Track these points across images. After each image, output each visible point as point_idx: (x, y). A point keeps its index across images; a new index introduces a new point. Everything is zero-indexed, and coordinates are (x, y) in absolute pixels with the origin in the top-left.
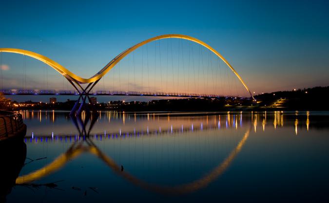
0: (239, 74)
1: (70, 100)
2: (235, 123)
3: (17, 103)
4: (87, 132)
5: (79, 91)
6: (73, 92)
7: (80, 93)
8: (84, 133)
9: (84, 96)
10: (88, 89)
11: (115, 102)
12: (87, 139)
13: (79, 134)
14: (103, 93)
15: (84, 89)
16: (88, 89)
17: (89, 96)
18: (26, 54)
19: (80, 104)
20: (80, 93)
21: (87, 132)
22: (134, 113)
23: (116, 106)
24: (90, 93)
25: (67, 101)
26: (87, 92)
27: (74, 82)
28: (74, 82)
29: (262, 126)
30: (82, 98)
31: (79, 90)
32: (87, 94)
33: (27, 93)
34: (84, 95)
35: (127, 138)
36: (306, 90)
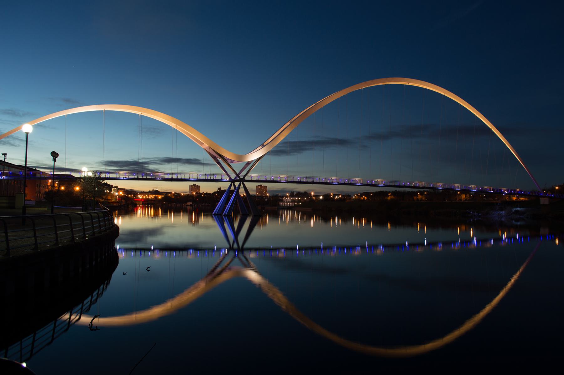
0: (506, 234)
6: (218, 177)
7: (230, 178)
8: (235, 246)
9: (237, 184)
10: (244, 173)
11: (299, 194)
13: (228, 246)
14: (401, 184)
16: (244, 173)
17: (245, 183)
20: (230, 178)
21: (241, 244)
22: (458, 201)
23: (299, 201)
24: (246, 178)
25: (216, 190)
26: (242, 177)
27: (220, 160)
28: (220, 160)
30: (234, 185)
32: (243, 180)
34: (237, 181)
36: (372, 193)
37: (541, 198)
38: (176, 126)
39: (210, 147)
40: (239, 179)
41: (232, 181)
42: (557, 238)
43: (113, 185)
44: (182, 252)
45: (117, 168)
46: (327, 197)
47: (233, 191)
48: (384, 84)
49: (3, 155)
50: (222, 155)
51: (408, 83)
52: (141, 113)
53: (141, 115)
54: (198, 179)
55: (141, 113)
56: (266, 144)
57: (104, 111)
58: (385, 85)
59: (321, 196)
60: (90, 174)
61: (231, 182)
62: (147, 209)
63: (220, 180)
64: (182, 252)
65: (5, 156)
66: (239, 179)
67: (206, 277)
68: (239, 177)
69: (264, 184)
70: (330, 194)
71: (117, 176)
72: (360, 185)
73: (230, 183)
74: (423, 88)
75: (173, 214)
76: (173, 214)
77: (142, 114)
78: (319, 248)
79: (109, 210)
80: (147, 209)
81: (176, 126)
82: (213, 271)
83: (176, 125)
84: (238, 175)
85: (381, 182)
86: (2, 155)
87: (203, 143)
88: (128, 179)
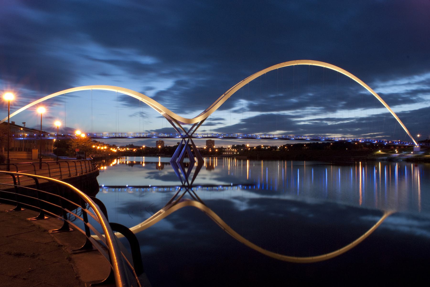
9: (187, 139)
27: (174, 122)
28: (174, 122)
32: (191, 137)
37: (189, 144)
38: (142, 99)
39: (166, 114)
40: (188, 136)
41: (184, 138)
42: (248, 179)
43: (100, 142)
44: (122, 189)
45: (410, 135)
46: (259, 148)
47: (183, 145)
48: (294, 65)
49: (23, 123)
50: (176, 120)
51: (311, 64)
52: (117, 91)
53: (117, 92)
54: (134, 137)
55: (117, 91)
56: (207, 110)
57: (91, 90)
58: (295, 65)
59: (118, 147)
60: (83, 136)
61: (182, 138)
62: (229, 159)
63: (127, 137)
64: (122, 189)
65: (24, 124)
66: (188, 136)
67: (166, 206)
68: (188, 135)
69: (212, 139)
70: (261, 146)
71: (164, 136)
72: (293, 140)
73: (181, 139)
74: (323, 67)
75: (242, 160)
76: (242, 160)
77: (118, 92)
78: (125, 187)
79: (92, 159)
80: (229, 159)
81: (142, 99)
82: (170, 202)
83: (142, 98)
84: (187, 134)
85: (293, 136)
86: (22, 123)
87: (162, 111)
88: (109, 138)
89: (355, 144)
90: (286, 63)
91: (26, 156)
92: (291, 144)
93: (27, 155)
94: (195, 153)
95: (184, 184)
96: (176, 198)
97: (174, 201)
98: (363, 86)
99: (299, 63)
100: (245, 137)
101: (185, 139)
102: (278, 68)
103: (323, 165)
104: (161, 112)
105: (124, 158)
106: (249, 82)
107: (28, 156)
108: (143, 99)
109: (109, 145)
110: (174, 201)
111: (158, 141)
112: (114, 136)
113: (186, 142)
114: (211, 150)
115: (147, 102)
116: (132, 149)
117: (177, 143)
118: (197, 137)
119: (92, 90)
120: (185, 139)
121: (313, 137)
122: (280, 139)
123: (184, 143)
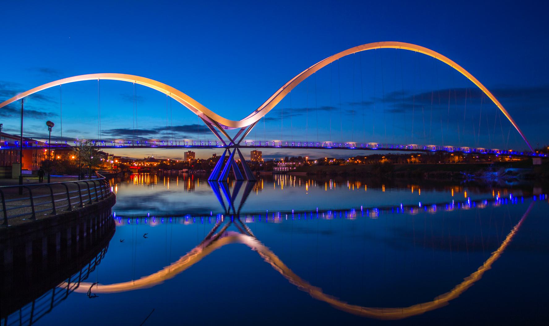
1: (103, 151)
2: (357, 184)
3: (204, 171)
4: (236, 210)
5: (223, 142)
6: (213, 144)
7: (225, 144)
9: (232, 150)
11: (294, 159)
12: (236, 221)
15: (232, 138)
18: (138, 82)
19: (20, 146)
21: (236, 210)
23: (294, 166)
24: (241, 144)
25: (211, 156)
29: (352, 188)
31: (224, 139)
32: (237, 146)
33: (312, 145)
34: (232, 147)
35: (191, 192)
38: (170, 93)
39: (204, 114)
50: (217, 122)
51: (380, 47)
52: (136, 82)
53: (135, 84)
58: (377, 49)
61: (225, 148)
66: (233, 144)
79: (105, 178)
81: (170, 93)
82: (209, 238)
83: (170, 92)
84: (232, 141)
87: (197, 110)
89: (274, 159)
90: (366, 45)
91: (3, 173)
92: (365, 157)
93: (4, 171)
94: (237, 167)
95: (227, 210)
96: (217, 230)
97: (215, 235)
98: (466, 78)
99: (383, 46)
100: (285, 145)
101: (229, 149)
102: (354, 53)
103: (13, 201)
104: (196, 112)
105: (147, 175)
106: (316, 71)
107: (6, 173)
108: (171, 93)
109: (120, 157)
110: (215, 235)
111: (187, 153)
112: (199, 145)
113: (231, 154)
114: (357, 161)
115: (174, 95)
116: (152, 163)
117: (212, 155)
118: (275, 146)
119: (99, 80)
120: (229, 149)
121: (21, 156)
122: (356, 148)
123: (227, 154)
